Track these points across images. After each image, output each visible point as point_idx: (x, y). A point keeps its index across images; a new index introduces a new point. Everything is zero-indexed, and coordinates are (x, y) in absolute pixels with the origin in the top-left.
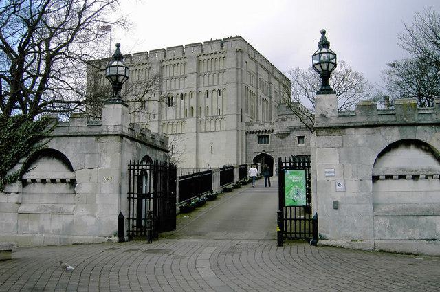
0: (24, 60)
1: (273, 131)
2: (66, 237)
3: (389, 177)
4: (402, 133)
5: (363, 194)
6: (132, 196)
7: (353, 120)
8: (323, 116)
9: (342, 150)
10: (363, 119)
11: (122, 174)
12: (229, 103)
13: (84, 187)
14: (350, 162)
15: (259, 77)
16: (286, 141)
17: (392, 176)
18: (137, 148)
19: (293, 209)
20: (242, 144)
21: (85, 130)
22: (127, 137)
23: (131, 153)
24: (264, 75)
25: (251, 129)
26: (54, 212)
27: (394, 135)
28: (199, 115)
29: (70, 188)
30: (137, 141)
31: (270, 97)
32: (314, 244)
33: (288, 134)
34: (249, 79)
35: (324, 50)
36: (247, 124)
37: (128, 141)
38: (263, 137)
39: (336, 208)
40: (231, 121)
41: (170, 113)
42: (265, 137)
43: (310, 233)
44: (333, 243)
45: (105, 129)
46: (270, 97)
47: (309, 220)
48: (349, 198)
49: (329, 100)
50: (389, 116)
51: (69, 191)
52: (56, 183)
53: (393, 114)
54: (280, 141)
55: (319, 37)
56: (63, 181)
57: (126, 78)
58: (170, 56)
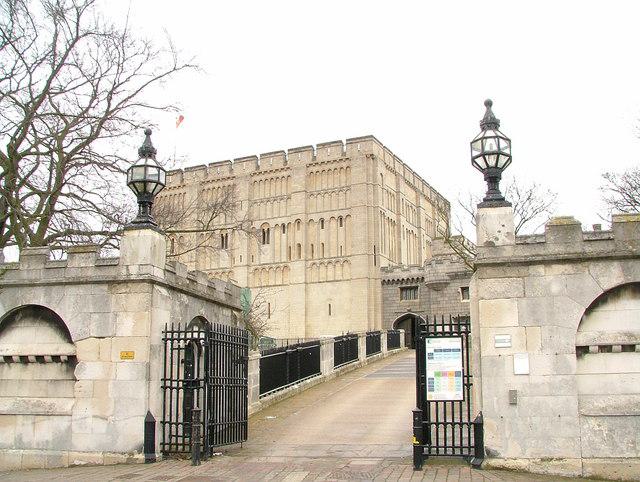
0: (18, 167)
2: (59, 453)
3: (606, 348)
4: (625, 271)
5: (560, 378)
6: (168, 383)
8: (490, 244)
9: (524, 301)
10: (554, 249)
11: (151, 348)
13: (88, 371)
14: (538, 323)
15: (402, 196)
16: (443, 295)
17: (611, 346)
18: (182, 303)
19: (441, 405)
20: (375, 299)
21: (92, 274)
23: (166, 312)
24: (409, 195)
25: (390, 276)
26: (40, 410)
27: (613, 275)
28: (310, 257)
29: (67, 371)
30: (182, 291)
32: (477, 467)
34: (386, 200)
35: (490, 133)
36: (383, 269)
37: (164, 291)
38: (408, 287)
39: (513, 404)
40: (360, 266)
41: (266, 255)
42: (411, 288)
43: (477, 452)
44: (510, 464)
45: (124, 271)
48: (536, 386)
49: (499, 216)
50: (604, 243)
51: (64, 377)
52: (13, 362)
53: (609, 239)
54: (434, 294)
55: (480, 113)
56: (56, 359)
57: (159, 187)
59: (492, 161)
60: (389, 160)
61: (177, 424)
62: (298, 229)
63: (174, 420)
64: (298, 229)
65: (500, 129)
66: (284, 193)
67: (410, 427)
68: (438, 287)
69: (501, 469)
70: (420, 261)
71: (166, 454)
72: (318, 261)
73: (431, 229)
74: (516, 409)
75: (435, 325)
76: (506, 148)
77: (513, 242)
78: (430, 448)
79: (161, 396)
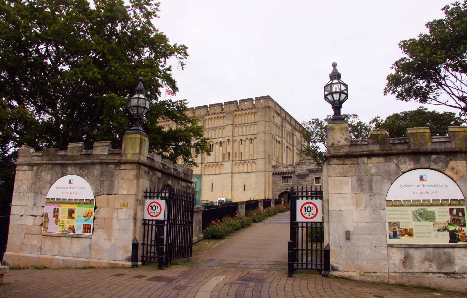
1: (294, 172)
7: (365, 148)
12: (258, 149)
14: (362, 191)
15: (284, 128)
16: (305, 181)
22: (145, 165)
24: (288, 128)
25: (277, 171)
31: (293, 145)
32: (326, 276)
33: (307, 175)
35: (336, 81)
36: (273, 167)
37: (146, 169)
38: (286, 176)
40: (261, 164)
43: (323, 266)
44: (346, 274)
46: (293, 145)
47: (321, 251)
54: (300, 181)
55: (330, 70)
58: (212, 111)
59: (336, 97)
60: (278, 110)
61: (151, 246)
62: (229, 144)
63: (149, 243)
64: (229, 144)
65: (341, 79)
66: (221, 125)
67: (286, 251)
68: (302, 177)
69: (339, 278)
70: (293, 163)
71: (144, 264)
72: (238, 162)
73: (299, 146)
74: (349, 243)
75: (302, 192)
76: (345, 90)
77: (349, 144)
78: (298, 264)
79: (142, 229)
